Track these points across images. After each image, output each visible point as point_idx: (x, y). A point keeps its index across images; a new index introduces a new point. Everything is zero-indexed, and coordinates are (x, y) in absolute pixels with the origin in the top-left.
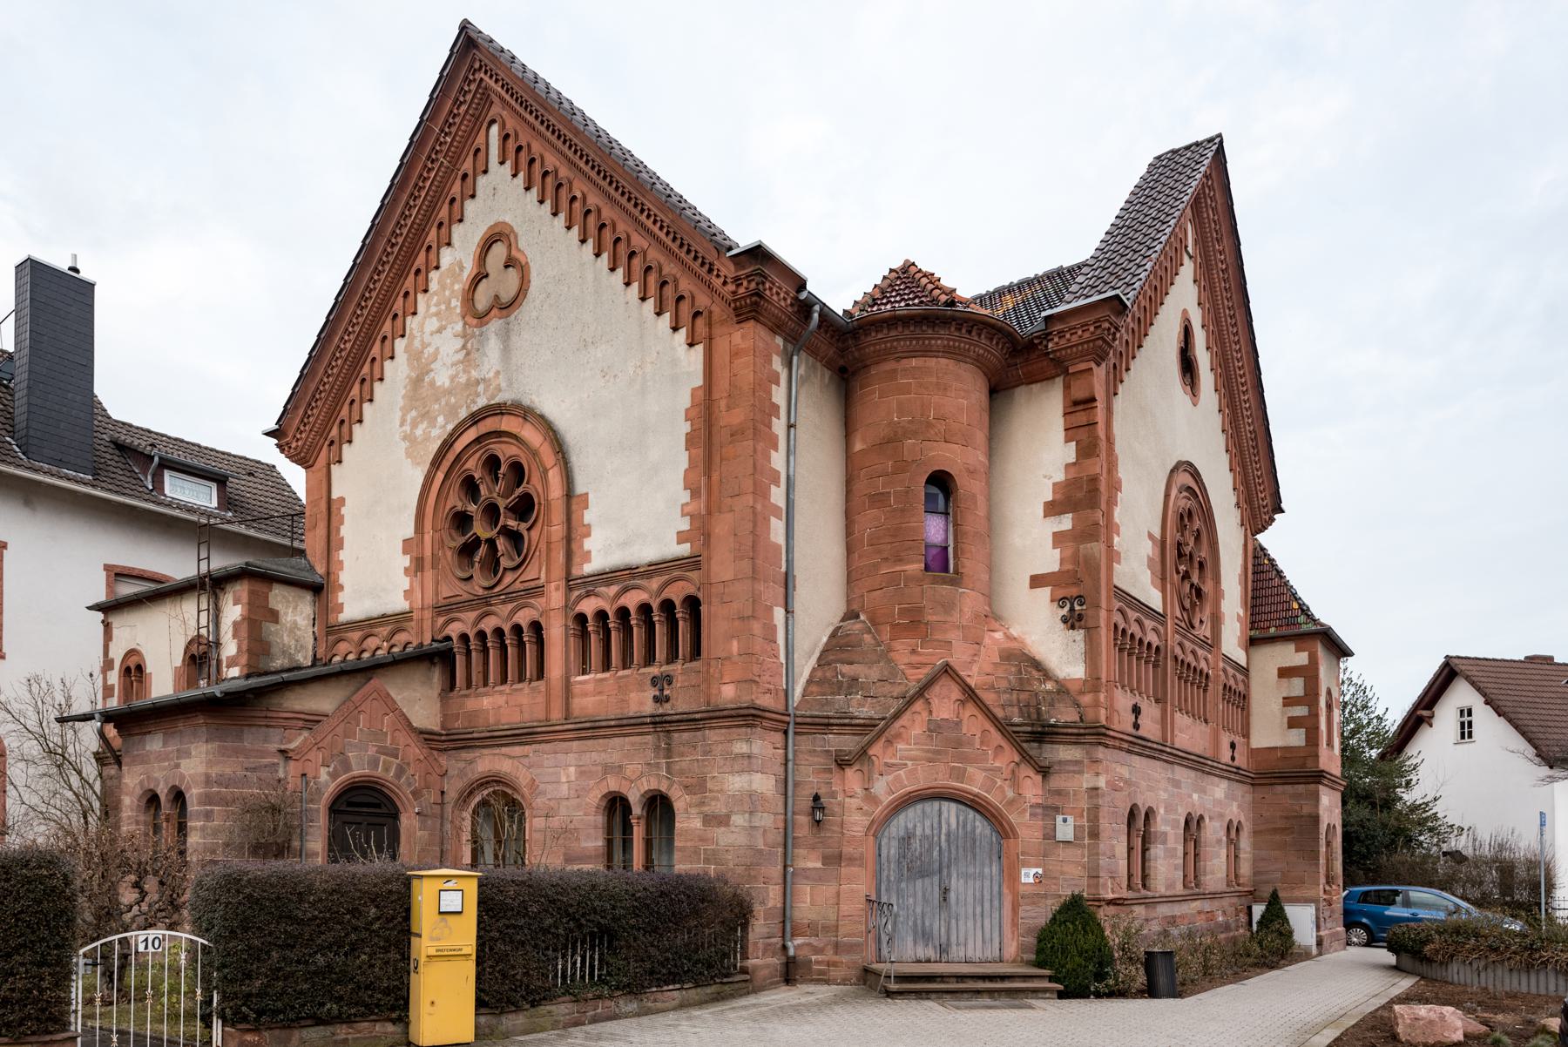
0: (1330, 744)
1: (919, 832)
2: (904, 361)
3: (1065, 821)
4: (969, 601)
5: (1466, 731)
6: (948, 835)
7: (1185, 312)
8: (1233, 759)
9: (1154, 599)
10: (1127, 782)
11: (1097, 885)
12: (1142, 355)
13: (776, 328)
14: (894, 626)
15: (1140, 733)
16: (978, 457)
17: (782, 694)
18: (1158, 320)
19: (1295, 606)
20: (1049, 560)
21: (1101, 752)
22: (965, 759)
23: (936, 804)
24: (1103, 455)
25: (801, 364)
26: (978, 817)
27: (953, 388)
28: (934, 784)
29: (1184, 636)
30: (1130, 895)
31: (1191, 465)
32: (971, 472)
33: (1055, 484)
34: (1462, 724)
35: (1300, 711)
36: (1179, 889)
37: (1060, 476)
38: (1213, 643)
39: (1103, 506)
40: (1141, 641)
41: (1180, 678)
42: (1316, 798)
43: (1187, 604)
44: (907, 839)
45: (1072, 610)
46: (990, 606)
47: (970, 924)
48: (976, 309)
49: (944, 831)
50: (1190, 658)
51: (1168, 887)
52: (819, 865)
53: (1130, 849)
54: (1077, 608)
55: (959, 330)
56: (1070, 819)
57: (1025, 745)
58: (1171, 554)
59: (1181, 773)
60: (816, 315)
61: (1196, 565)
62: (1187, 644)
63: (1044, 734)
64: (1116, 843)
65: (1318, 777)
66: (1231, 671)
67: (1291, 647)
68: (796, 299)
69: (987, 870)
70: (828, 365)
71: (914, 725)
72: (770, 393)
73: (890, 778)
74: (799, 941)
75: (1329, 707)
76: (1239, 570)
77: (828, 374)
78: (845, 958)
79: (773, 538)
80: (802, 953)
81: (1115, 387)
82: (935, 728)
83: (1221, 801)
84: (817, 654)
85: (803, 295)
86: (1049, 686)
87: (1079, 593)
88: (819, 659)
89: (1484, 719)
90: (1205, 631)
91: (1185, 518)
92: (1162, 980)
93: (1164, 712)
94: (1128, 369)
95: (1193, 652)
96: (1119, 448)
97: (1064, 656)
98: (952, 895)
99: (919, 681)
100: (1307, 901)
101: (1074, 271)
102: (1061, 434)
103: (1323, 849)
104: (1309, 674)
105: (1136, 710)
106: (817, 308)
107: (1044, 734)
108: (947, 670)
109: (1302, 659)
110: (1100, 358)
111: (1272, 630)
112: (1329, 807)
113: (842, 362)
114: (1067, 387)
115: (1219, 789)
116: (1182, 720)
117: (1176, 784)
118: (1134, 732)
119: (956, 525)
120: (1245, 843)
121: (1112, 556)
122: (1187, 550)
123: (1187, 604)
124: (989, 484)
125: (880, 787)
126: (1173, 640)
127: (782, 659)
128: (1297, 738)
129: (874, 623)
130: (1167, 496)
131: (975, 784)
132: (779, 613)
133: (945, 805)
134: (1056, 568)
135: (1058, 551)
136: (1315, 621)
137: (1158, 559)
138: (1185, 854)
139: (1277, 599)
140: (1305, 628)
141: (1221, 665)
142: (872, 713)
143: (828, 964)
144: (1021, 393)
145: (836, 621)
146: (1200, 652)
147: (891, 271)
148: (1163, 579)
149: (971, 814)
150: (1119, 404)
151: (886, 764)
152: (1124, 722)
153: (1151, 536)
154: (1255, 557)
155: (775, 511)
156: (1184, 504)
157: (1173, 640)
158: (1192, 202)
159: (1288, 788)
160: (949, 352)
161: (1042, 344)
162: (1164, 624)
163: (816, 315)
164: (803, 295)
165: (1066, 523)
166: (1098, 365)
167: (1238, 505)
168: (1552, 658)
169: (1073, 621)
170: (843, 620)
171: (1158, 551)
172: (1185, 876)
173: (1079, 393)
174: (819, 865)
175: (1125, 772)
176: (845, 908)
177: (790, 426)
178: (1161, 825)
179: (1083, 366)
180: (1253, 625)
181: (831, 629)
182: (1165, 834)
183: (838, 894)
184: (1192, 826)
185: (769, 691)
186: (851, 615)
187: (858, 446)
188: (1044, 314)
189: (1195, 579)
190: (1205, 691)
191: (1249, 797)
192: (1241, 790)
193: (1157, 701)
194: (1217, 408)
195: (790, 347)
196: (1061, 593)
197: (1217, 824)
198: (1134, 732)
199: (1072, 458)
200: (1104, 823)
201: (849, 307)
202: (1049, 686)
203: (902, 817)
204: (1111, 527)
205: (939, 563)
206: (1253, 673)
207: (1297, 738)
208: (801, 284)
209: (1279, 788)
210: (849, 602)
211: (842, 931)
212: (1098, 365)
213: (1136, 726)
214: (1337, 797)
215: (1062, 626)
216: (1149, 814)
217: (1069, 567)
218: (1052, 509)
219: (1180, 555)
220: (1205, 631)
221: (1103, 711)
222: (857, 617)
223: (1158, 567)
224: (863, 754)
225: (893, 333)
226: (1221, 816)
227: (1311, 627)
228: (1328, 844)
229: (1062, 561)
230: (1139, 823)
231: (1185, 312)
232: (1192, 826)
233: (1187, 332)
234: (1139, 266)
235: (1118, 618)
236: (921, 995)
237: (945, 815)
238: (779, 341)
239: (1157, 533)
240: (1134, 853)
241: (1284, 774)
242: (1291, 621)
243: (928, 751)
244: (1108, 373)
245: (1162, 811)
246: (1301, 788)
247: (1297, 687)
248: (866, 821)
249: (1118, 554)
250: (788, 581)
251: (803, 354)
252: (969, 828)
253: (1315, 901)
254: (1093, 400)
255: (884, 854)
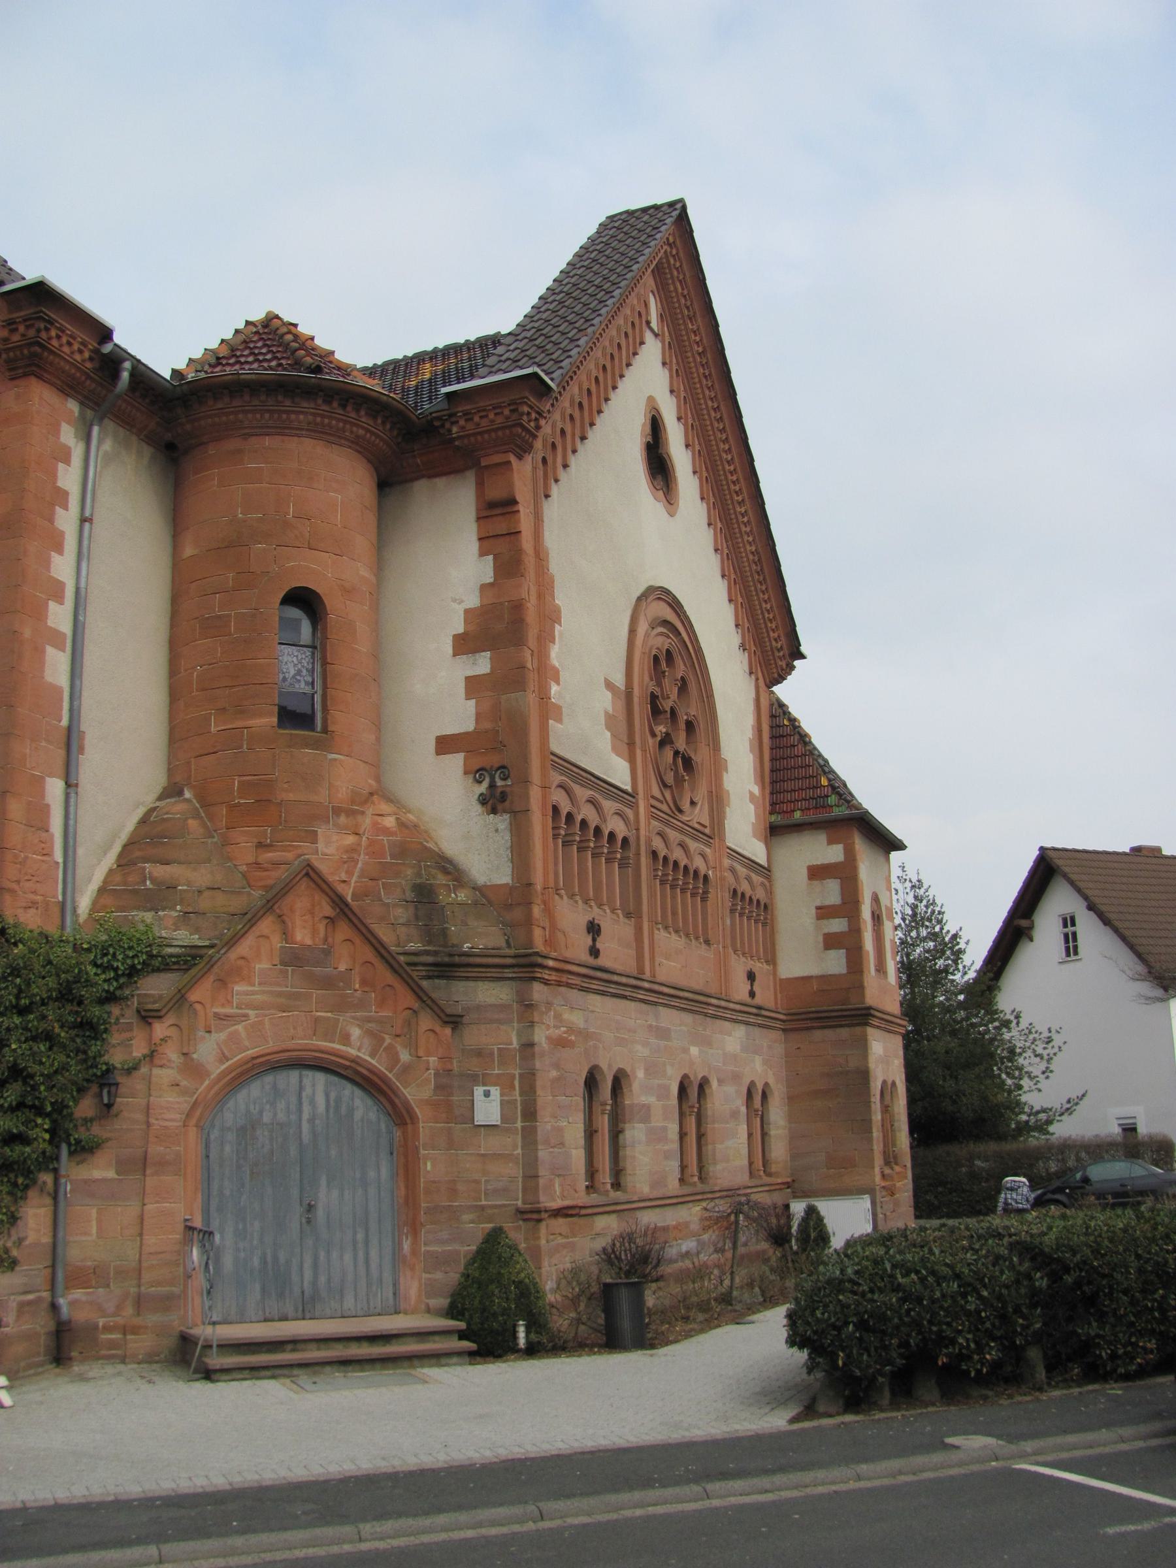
0: (881, 968)
1: (267, 1118)
2: (253, 440)
3: (487, 1094)
4: (344, 774)
5: (1071, 945)
6: (312, 1120)
7: (651, 399)
8: (752, 994)
9: (619, 772)
10: (585, 1035)
11: (536, 1188)
12: (587, 451)
13: (68, 387)
14: (232, 807)
15: (602, 961)
16: (360, 571)
17: (56, 911)
18: (610, 409)
19: (824, 782)
20: (461, 716)
21: (538, 992)
22: (341, 1006)
23: (294, 1075)
24: (531, 573)
25: (105, 440)
26: (358, 1092)
27: (332, 482)
28: (290, 1044)
29: (667, 823)
30: (594, 1198)
31: (667, 592)
32: (348, 591)
33: (467, 611)
34: (1066, 936)
35: (838, 925)
36: (673, 1186)
37: (473, 601)
38: (712, 833)
39: (532, 641)
40: (598, 831)
41: (663, 882)
42: (863, 1045)
43: (670, 778)
44: (247, 1130)
45: (492, 786)
46: (378, 779)
47: (348, 1257)
48: (374, 385)
49: (305, 1116)
50: (677, 854)
51: (654, 1185)
52: (111, 1174)
53: (590, 1134)
54: (499, 783)
55: (344, 406)
56: (495, 1092)
57: (425, 984)
58: (641, 710)
59: (668, 1018)
60: (125, 375)
61: (683, 726)
62: (673, 835)
63: (451, 966)
64: (565, 1124)
65: (863, 1016)
66: (742, 871)
67: (822, 837)
68: (97, 351)
69: (372, 1174)
70: (150, 439)
71: (260, 950)
72: (54, 476)
73: (223, 1036)
74: (78, 1294)
75: (877, 918)
76: (749, 733)
77: (148, 451)
78: (152, 1319)
79: (49, 677)
80: (81, 1316)
81: (547, 487)
82: (294, 959)
83: (738, 1057)
84: (117, 849)
85: (107, 348)
86: (462, 896)
87: (500, 759)
88: (121, 855)
89: (1089, 929)
90: (699, 815)
91: (661, 662)
92: (626, 1324)
93: (639, 930)
94: (565, 466)
95: (682, 845)
96: (555, 566)
97: (476, 846)
98: (320, 1213)
99: (267, 888)
100: (859, 1191)
101: (495, 340)
102: (474, 546)
103: (877, 1117)
104: (846, 873)
105: (594, 929)
106: (127, 365)
107: (451, 966)
108: (310, 873)
109: (834, 854)
110: (523, 449)
111: (797, 814)
112: (885, 1057)
113: (168, 436)
114: (480, 484)
115: (733, 1039)
116: (668, 941)
117: (663, 1034)
118: (591, 961)
119: (325, 663)
120: (777, 1114)
121: (548, 711)
122: (667, 705)
123: (670, 778)
124: (376, 607)
125: (207, 1050)
126: (648, 828)
127: (59, 856)
128: (835, 963)
129: (205, 803)
130: (632, 631)
131: (356, 1045)
132: (55, 788)
133: (309, 1075)
134: (469, 725)
135: (472, 703)
136: (858, 806)
137: (622, 717)
138: (682, 1135)
139: (802, 772)
140: (837, 812)
141: (727, 862)
142: (195, 940)
143: (125, 1330)
144: (421, 487)
145: (149, 800)
146: (693, 845)
147: (248, 323)
148: (631, 744)
149: (348, 1089)
150: (553, 510)
151: (217, 1016)
152: (577, 946)
153: (609, 685)
154: (773, 716)
155: (56, 639)
156: (661, 642)
157: (648, 828)
158: (645, 270)
159: (829, 1033)
160: (319, 432)
161: (456, 428)
162: (634, 806)
163: (125, 375)
164: (107, 348)
165: (482, 664)
166: (520, 458)
167: (743, 647)
168: (1159, 849)
169: (493, 802)
170: (160, 798)
171: (621, 704)
172: (683, 1168)
173: (495, 492)
174: (111, 1174)
175: (576, 1019)
176: (152, 1241)
177: (84, 520)
178: (638, 1094)
179: (497, 458)
180: (774, 807)
181: (140, 812)
182: (647, 1108)
183: (141, 1219)
184: (692, 1094)
185: (34, 904)
186: (172, 791)
187: (189, 551)
188: (444, 390)
189: (681, 743)
190: (704, 899)
191: (779, 1049)
192: (771, 1043)
193: (628, 915)
194: (705, 521)
195: (89, 413)
196: (477, 763)
197: (730, 1089)
198: (591, 961)
199: (489, 577)
200: (544, 1098)
201: (181, 365)
202: (462, 896)
203: (242, 1096)
204: (548, 674)
205: (295, 717)
206: (778, 874)
207: (835, 963)
208: (105, 334)
209: (818, 1034)
210: (171, 771)
211: (146, 1277)
212: (520, 458)
213: (594, 952)
214: (897, 1043)
215: (479, 808)
216: (619, 1082)
217: (487, 725)
218: (464, 645)
219: (656, 711)
220: (699, 815)
221: (537, 933)
222: (180, 793)
223: (623, 727)
224: (180, 1000)
225: (220, 405)
226: (736, 1077)
227: (840, 811)
228: (886, 1109)
229: (479, 717)
230: (605, 1094)
231: (651, 399)
232: (692, 1094)
233: (656, 426)
234: (572, 341)
235: (559, 797)
236: (255, 1372)
237: (308, 1091)
238: (73, 406)
239: (619, 680)
240: (688, 1138)
241: (826, 1013)
242: (820, 804)
243: (280, 994)
244: (535, 468)
245: (640, 1074)
246: (844, 1033)
247: (831, 893)
248: (185, 1103)
249: (558, 709)
250: (71, 741)
251: (110, 425)
252: (343, 1110)
253: (870, 1191)
254: (514, 502)
255: (213, 1154)
